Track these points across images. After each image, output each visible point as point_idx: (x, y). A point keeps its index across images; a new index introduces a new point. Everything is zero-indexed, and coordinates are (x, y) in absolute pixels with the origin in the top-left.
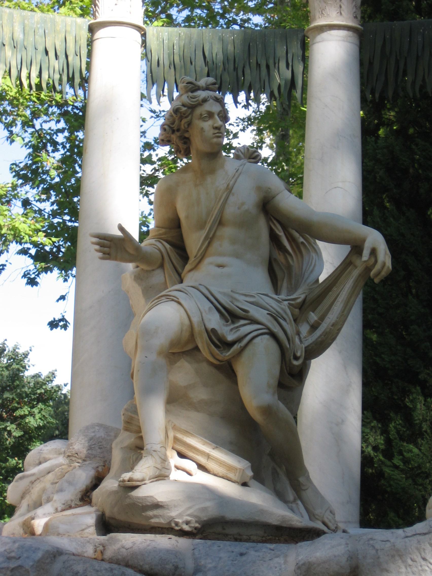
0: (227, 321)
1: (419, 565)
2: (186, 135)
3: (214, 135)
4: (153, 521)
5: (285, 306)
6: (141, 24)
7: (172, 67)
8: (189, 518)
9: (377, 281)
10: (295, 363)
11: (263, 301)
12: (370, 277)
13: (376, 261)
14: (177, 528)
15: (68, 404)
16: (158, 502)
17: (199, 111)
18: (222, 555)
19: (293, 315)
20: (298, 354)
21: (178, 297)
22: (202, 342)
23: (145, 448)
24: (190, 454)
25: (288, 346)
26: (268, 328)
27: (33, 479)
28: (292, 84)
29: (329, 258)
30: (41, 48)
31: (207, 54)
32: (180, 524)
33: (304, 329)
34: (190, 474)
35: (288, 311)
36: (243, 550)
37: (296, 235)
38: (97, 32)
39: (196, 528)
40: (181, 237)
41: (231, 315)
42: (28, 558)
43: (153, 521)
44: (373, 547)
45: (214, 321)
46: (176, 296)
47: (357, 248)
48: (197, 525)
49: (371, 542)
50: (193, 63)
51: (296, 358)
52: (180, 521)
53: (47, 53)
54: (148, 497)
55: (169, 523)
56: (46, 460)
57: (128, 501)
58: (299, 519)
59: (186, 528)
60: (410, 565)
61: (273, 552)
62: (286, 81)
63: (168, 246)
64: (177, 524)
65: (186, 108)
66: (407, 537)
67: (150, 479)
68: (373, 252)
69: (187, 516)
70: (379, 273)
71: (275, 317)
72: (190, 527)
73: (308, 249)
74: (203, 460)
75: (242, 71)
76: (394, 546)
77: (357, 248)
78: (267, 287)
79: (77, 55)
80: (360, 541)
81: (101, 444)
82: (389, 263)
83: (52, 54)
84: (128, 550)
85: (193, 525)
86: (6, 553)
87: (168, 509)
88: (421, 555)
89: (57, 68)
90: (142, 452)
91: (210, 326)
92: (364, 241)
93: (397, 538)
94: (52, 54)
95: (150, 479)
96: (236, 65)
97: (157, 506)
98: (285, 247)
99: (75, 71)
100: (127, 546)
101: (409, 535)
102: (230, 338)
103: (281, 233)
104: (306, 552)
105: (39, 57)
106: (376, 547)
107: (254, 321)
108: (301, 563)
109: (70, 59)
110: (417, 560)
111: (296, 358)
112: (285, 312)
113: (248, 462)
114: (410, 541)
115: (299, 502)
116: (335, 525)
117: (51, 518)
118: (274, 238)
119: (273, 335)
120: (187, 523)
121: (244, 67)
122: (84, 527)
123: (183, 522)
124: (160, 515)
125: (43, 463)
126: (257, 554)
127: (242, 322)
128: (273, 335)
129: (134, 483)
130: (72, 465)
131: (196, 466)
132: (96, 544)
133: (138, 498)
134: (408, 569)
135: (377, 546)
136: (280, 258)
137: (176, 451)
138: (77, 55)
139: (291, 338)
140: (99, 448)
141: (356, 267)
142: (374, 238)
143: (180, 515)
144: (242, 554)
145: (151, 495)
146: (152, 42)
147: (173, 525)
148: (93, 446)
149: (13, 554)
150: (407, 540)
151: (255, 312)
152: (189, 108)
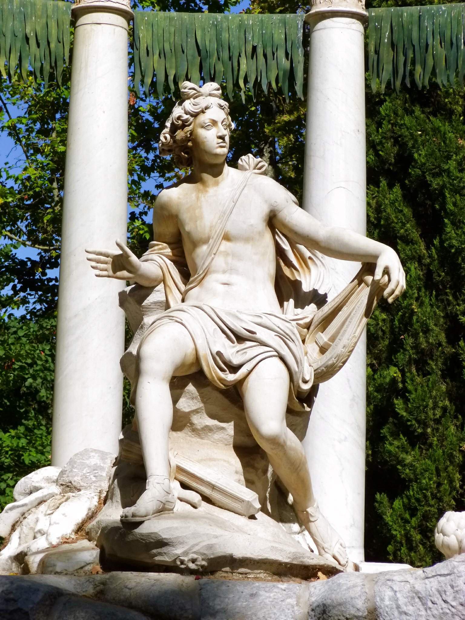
0: (233, 342)
1: (440, 607)
3: (218, 145)
4: (157, 558)
5: (293, 326)
6: (129, 9)
7: (162, 56)
8: (195, 556)
9: (390, 300)
11: (269, 321)
12: (383, 296)
13: (389, 280)
14: (183, 566)
16: (163, 539)
19: (301, 335)
20: (307, 378)
21: (182, 319)
24: (194, 484)
25: (297, 369)
26: (276, 351)
27: (25, 509)
28: (291, 75)
30: (20, 35)
31: (199, 41)
32: (185, 562)
33: (312, 349)
34: (195, 507)
37: (302, 248)
38: (80, 17)
39: (202, 566)
43: (157, 558)
46: (178, 316)
48: (204, 563)
49: (389, 583)
50: (185, 51)
51: (306, 382)
52: (186, 559)
53: (27, 39)
54: (152, 533)
55: (175, 561)
56: (37, 489)
57: (130, 537)
59: (192, 566)
60: (430, 608)
61: (284, 592)
62: (285, 72)
64: (182, 562)
65: (188, 116)
66: (427, 578)
67: (153, 514)
68: (386, 272)
69: (192, 553)
70: (393, 292)
71: (284, 337)
72: (197, 565)
73: (316, 264)
74: (207, 491)
75: (237, 60)
76: (414, 588)
77: (369, 267)
79: (60, 42)
80: (377, 581)
81: (96, 472)
82: (403, 283)
83: (33, 42)
84: (132, 591)
85: (199, 563)
86: (4, 594)
87: (173, 546)
88: (441, 596)
89: (38, 57)
93: (416, 579)
94: (33, 42)
95: (153, 514)
96: (231, 54)
97: (162, 543)
99: (57, 59)
100: (130, 586)
101: (430, 576)
102: (236, 361)
103: (286, 246)
104: (318, 589)
105: (18, 45)
106: (395, 589)
108: (315, 605)
109: (52, 45)
110: (437, 602)
111: (306, 382)
113: (255, 493)
114: (430, 582)
115: (306, 532)
116: (346, 560)
117: (47, 554)
118: (280, 253)
119: (282, 359)
120: (193, 561)
121: (240, 56)
122: (83, 564)
123: (189, 560)
124: (165, 553)
125: (35, 492)
126: (267, 594)
128: (282, 359)
129: (137, 518)
130: (65, 495)
131: (200, 498)
132: (97, 583)
133: (142, 535)
134: (428, 611)
135: (396, 588)
136: (287, 271)
137: (179, 482)
138: (60, 42)
139: (299, 361)
140: (95, 476)
142: (388, 257)
143: (186, 553)
145: (155, 531)
146: (143, 34)
147: (179, 563)
148: (88, 474)
149: (12, 596)
150: (427, 581)
151: (262, 334)
152: (192, 116)
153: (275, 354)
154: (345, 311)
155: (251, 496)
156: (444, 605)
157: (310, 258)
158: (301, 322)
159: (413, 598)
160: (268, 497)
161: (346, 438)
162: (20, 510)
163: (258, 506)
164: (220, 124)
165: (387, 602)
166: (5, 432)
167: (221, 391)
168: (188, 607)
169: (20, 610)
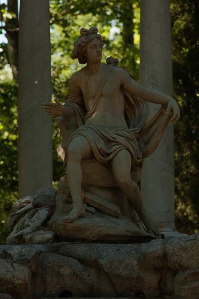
2: (85, 55)
10: (139, 161)
13: (173, 114)
15: (17, 154)
17: (89, 45)
18: (109, 250)
22: (97, 154)
23: (74, 202)
26: (125, 146)
29: (152, 110)
35: (134, 137)
36: (118, 248)
40: (83, 101)
41: (108, 141)
42: (29, 255)
44: (172, 245)
45: (102, 145)
47: (165, 106)
51: (138, 159)
56: (24, 207)
58: (142, 230)
59: (94, 239)
63: (77, 106)
66: (186, 241)
78: (126, 126)
90: (72, 205)
91: (100, 146)
92: (167, 104)
98: (131, 102)
107: (119, 143)
111: (138, 159)
112: (133, 138)
120: (94, 237)
127: (113, 144)
128: (128, 150)
141: (164, 115)
144: (118, 250)
147: (88, 238)
149: (22, 254)
152: (85, 43)
153: (124, 147)
154: (155, 126)
155: (116, 209)
156: (192, 252)
157: (140, 100)
158: (136, 132)
159: (181, 249)
160: (136, 31)
161: (164, 169)
162: (17, 216)
163: (119, 212)
164: (98, 46)
165: (171, 251)
166: (165, 268)
167: (102, 164)
168: (93, 255)
169: (27, 259)
